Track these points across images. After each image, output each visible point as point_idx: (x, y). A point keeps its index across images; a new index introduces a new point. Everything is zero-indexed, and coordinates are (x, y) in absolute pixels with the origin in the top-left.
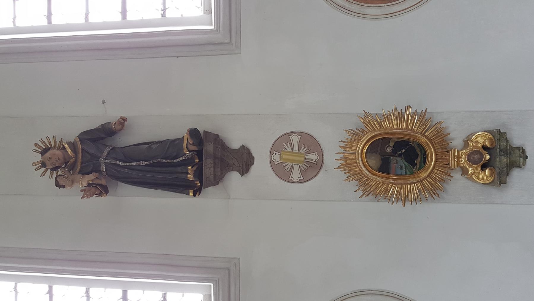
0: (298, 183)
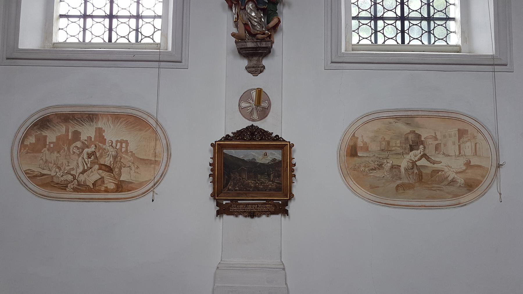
0: (239, 105)
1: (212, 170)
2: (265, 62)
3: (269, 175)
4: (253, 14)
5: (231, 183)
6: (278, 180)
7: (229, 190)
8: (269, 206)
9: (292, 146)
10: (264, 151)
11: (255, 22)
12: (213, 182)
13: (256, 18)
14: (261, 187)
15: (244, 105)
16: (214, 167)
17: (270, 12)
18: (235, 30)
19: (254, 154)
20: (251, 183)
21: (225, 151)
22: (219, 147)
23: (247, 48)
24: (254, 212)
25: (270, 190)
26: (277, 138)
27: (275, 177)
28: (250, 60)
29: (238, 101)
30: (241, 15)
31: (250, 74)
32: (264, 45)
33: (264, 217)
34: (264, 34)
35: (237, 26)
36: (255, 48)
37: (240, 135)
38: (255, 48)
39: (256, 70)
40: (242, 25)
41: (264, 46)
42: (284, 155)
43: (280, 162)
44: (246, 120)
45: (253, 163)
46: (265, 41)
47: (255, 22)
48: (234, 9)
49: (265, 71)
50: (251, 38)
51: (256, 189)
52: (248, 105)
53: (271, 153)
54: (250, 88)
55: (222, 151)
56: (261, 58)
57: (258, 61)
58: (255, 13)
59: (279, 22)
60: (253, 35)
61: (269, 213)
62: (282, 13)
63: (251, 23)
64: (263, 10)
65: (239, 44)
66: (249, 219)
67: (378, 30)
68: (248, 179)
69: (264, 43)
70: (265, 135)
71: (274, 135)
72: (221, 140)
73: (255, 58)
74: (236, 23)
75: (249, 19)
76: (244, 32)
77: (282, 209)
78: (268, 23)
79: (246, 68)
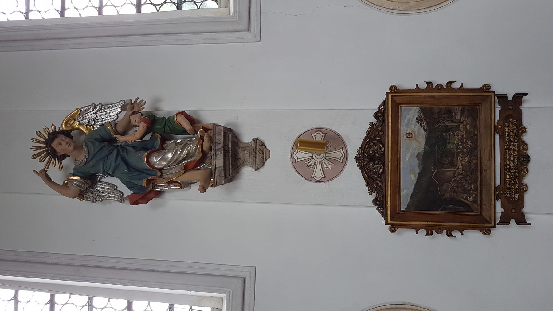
0: (319, 181)
1: (439, 232)
2: (247, 138)
3: (448, 130)
4: (170, 155)
5: (462, 197)
6: (457, 114)
7: (475, 202)
8: (507, 128)
9: (394, 89)
10: (403, 138)
11: (182, 152)
12: (461, 230)
14: (469, 143)
15: (318, 174)
16: (433, 227)
17: (167, 129)
18: (195, 188)
19: (408, 156)
20: (461, 161)
21: (403, 207)
22: (397, 220)
23: (225, 166)
24: (520, 155)
25: (475, 127)
26: (380, 115)
27: (450, 119)
28: (244, 164)
29: (312, 183)
30: (171, 176)
31: (266, 163)
32: (220, 138)
33: (526, 138)
34: (202, 138)
35: (188, 185)
36: (224, 155)
37: (374, 181)
38: (224, 155)
39: (260, 153)
40: (188, 174)
42: (410, 104)
43: (423, 110)
44: (345, 170)
45: (425, 158)
46: (214, 135)
47: (182, 152)
48: (161, 189)
49: (261, 138)
50: (208, 161)
51: (473, 152)
52: (319, 167)
53: (407, 125)
54: (290, 162)
55: (403, 213)
56: (241, 145)
57: (245, 149)
58: (169, 152)
59: (183, 113)
60: (204, 156)
61: (521, 130)
62: (169, 112)
63: (184, 159)
64: (164, 140)
65: (218, 181)
66: (531, 166)
67: (151, 303)
68: (455, 166)
69: (217, 137)
70: (374, 137)
71: (374, 120)
72: (384, 214)
73: (241, 154)
74: (183, 185)
75: (178, 162)
76: (198, 171)
77: (513, 106)
78: (183, 132)
79: (257, 169)
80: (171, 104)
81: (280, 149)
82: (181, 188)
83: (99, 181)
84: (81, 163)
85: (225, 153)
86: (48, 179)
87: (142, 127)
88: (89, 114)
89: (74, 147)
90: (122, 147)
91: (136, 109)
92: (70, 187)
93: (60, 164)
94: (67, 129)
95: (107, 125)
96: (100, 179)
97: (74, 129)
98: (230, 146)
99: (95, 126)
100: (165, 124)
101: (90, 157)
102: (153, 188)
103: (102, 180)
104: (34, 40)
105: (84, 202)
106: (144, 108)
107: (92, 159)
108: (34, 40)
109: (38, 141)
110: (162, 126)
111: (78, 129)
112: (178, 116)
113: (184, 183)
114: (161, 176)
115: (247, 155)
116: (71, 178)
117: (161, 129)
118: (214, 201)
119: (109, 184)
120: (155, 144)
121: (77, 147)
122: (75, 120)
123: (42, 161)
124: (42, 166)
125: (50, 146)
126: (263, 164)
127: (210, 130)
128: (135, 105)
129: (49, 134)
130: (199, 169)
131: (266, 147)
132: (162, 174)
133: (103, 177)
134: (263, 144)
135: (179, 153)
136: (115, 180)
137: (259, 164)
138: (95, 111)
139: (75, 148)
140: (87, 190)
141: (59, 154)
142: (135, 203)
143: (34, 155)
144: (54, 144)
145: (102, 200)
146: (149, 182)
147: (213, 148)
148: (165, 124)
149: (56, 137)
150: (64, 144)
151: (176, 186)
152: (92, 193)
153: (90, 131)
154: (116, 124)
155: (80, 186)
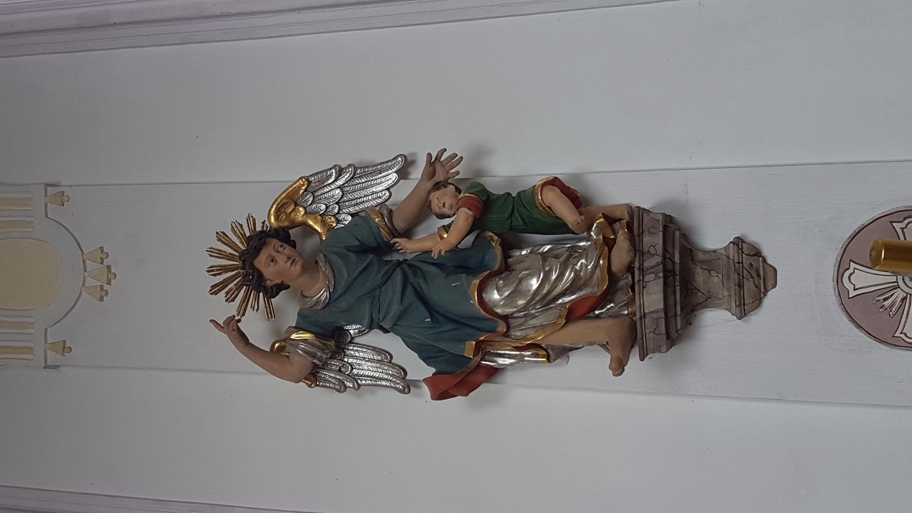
2: (713, 237)
13: (547, 275)
17: (518, 221)
28: (709, 301)
30: (531, 333)
31: (766, 301)
32: (653, 241)
41: (659, 239)
47: (561, 276)
49: (753, 237)
50: (622, 297)
54: (833, 298)
56: (701, 256)
58: (530, 276)
59: (554, 182)
62: (512, 180)
63: (563, 294)
64: (508, 247)
65: (651, 345)
69: (647, 239)
73: (700, 278)
74: (553, 353)
75: (546, 300)
78: (557, 226)
80: (517, 164)
81: (804, 269)
82: (549, 360)
83: (351, 342)
84: (317, 302)
85: (665, 277)
86: (242, 339)
87: (463, 218)
88: (326, 190)
89: (303, 266)
90: (410, 266)
91: (439, 177)
92: (291, 356)
93: (269, 305)
94: (281, 224)
95: (373, 216)
96: (352, 338)
97: (294, 225)
98: (677, 260)
99: (342, 217)
100: (513, 211)
101: (339, 291)
102: (482, 360)
103: (357, 340)
104: (190, 19)
105: (318, 393)
106: (458, 173)
107: (345, 292)
108: (190, 19)
109: (220, 254)
110: (506, 215)
111: (304, 224)
112: (546, 189)
113: (553, 348)
114: (506, 335)
115: (716, 279)
116: (294, 336)
117: (505, 221)
118: (818, 403)
119: (374, 349)
120: (487, 258)
121: (310, 266)
122: (296, 205)
123: (230, 299)
124: (232, 309)
125: (252, 267)
126: (758, 301)
127: (633, 220)
128: (438, 166)
129: (249, 240)
130: (598, 317)
131: (764, 260)
132: (508, 328)
133: (361, 333)
134: (757, 253)
135: (554, 277)
136: (393, 343)
137: (747, 301)
138: (340, 183)
139: (305, 269)
140: (324, 366)
141: (269, 283)
142: (440, 394)
143: (213, 287)
144: (261, 262)
145: (359, 386)
146: (479, 345)
147: (637, 265)
148: (513, 211)
149: (264, 244)
150: (281, 259)
151: (537, 356)
152: (340, 370)
153: (330, 229)
154: (390, 212)
155: (313, 356)
